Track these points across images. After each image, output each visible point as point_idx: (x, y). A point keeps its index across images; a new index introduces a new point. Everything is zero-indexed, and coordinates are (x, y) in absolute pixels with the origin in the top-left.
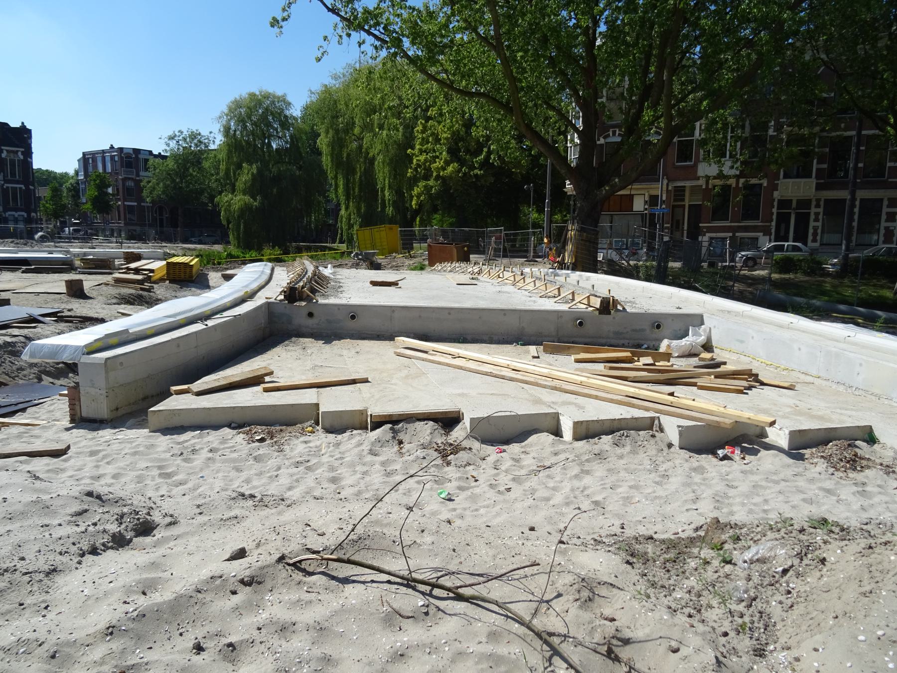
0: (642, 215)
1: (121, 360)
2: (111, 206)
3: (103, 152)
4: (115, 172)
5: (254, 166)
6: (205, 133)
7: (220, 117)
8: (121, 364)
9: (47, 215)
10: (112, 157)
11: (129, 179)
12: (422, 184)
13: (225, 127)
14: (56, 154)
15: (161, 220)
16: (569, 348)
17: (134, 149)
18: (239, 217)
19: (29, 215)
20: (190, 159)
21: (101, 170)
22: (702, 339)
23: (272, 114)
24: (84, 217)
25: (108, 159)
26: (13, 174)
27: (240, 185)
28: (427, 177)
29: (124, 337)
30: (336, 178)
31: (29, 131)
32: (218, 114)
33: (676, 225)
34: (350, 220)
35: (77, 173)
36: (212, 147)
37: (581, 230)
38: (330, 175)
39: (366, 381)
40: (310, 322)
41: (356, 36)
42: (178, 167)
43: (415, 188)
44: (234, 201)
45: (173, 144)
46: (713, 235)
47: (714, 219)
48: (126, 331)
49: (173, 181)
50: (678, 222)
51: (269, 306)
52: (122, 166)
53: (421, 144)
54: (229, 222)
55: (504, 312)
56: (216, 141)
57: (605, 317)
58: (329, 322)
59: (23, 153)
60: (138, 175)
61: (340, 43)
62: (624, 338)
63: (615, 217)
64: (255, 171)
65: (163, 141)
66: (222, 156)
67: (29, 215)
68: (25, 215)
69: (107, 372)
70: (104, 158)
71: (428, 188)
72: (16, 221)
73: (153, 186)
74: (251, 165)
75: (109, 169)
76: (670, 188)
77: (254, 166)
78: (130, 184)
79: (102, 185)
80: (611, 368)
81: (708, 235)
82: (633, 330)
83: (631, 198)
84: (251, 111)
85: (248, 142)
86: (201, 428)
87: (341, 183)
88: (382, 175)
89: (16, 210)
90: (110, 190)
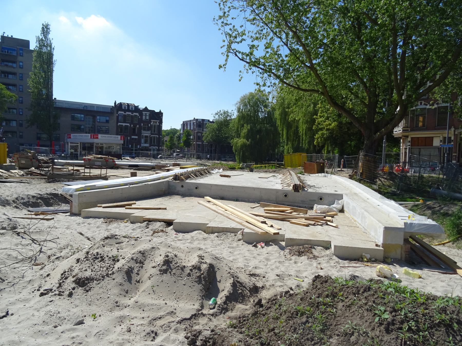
0: (439, 149)
1: (85, 194)
2: (191, 144)
3: (190, 121)
4: (194, 130)
5: (249, 126)
6: (230, 111)
7: (237, 104)
8: (85, 196)
9: (167, 148)
10: (194, 123)
11: (199, 132)
12: (320, 133)
13: (238, 108)
14: (171, 123)
15: (211, 150)
16: (269, 205)
18: (240, 148)
19: (159, 148)
20: (223, 124)
21: (189, 128)
22: (339, 207)
23: (260, 101)
24: (181, 148)
25: (192, 124)
26: (154, 131)
27: (242, 134)
28: (321, 129)
29: (93, 188)
30: (283, 130)
31: (162, 113)
32: (236, 102)
34: (288, 150)
35: (180, 130)
36: (233, 117)
37: (365, 156)
38: (280, 129)
39: (166, 209)
40: (182, 189)
41: (254, 69)
42: (218, 127)
43: (317, 135)
44: (238, 142)
45: (217, 117)
48: (95, 185)
49: (216, 133)
51: (168, 181)
52: (197, 127)
53: (321, 113)
55: (254, 189)
56: (235, 115)
57: (297, 193)
58: (189, 189)
59: (159, 122)
60: (203, 131)
61: (247, 73)
62: (306, 204)
63: (422, 149)
64: (249, 128)
65: (213, 115)
66: (237, 121)
67: (159, 148)
68: (157, 148)
69: (79, 198)
70: (190, 123)
71: (323, 134)
72: (154, 150)
73: (207, 135)
74: (247, 125)
75: (192, 128)
76: (456, 133)
77: (249, 126)
78: (199, 134)
79: (188, 135)
80: (266, 213)
82: (310, 200)
83: (431, 139)
84: (249, 100)
85: (248, 115)
86: (95, 218)
87: (285, 133)
88: (302, 127)
89: (154, 146)
90: (192, 137)
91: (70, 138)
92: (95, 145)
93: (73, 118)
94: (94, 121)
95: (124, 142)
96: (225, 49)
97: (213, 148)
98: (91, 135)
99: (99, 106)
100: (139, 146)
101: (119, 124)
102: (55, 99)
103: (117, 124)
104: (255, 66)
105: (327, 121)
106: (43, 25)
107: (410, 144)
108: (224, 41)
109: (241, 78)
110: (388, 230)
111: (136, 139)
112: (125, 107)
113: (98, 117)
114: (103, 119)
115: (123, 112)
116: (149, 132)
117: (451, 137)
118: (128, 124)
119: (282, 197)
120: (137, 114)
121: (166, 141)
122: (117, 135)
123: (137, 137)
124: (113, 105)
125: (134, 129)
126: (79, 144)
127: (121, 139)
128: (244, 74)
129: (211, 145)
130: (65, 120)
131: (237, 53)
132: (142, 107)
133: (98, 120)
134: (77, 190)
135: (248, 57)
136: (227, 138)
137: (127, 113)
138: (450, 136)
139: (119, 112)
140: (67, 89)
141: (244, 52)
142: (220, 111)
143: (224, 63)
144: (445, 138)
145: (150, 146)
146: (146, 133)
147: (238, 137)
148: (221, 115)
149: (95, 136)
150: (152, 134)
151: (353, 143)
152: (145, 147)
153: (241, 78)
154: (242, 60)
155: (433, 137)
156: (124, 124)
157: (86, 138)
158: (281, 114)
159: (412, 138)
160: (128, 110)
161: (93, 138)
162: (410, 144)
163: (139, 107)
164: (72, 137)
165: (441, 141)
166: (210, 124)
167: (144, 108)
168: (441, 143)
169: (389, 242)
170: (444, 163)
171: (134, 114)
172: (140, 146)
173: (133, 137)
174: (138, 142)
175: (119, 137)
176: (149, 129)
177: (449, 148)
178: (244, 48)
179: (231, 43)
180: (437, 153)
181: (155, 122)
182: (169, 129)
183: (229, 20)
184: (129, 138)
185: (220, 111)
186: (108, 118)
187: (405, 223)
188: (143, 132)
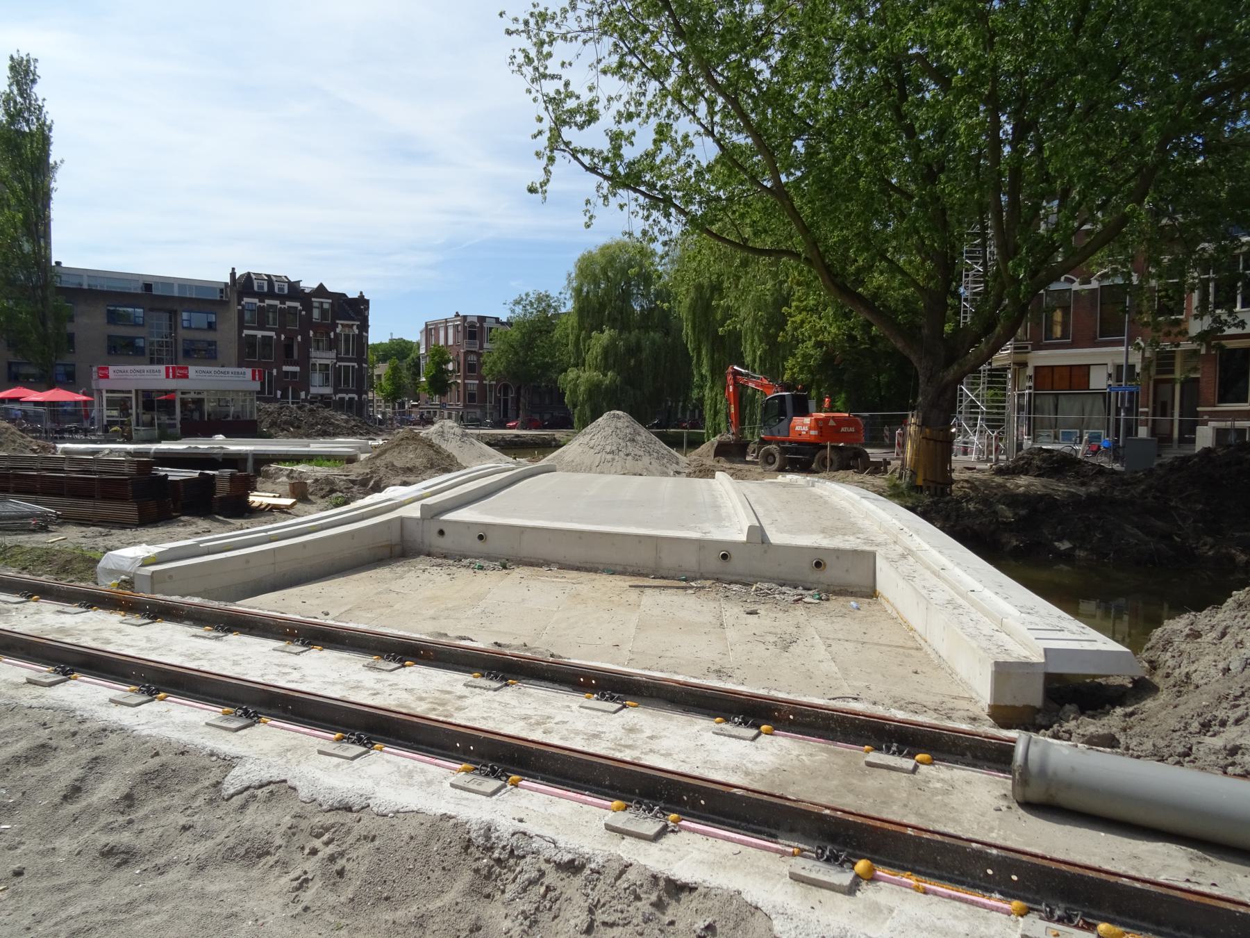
0: (1105, 396)
3: (446, 321)
6: (554, 294)
8: (171, 577)
11: (472, 352)
17: (479, 317)
20: (537, 328)
21: (442, 342)
27: (589, 358)
31: (367, 302)
33: (1162, 408)
36: (563, 310)
37: (923, 424)
41: (625, 195)
45: (519, 309)
46: (1222, 425)
47: (1223, 399)
49: (516, 353)
50: (1164, 405)
51: (402, 520)
54: (575, 406)
59: (358, 327)
60: (481, 347)
75: (451, 342)
78: (473, 358)
81: (1212, 424)
89: (347, 392)
90: (450, 366)
91: (106, 377)
92: (178, 396)
93: (113, 318)
94: (173, 326)
95: (263, 384)
96: (543, 140)
97: (511, 395)
98: (167, 369)
99: (184, 284)
100: (303, 395)
101: (246, 332)
102: (58, 263)
103: (240, 332)
104: (627, 187)
105: (817, 324)
106: (12, 58)
107: (1031, 384)
108: (540, 120)
109: (591, 217)
110: (1004, 672)
111: (296, 373)
112: (261, 287)
113: (185, 315)
114: (200, 319)
115: (256, 301)
116: (333, 354)
117: (1133, 366)
118: (273, 334)
119: (714, 564)
120: (297, 304)
121: (379, 376)
122: (240, 366)
123: (297, 369)
124: (228, 280)
125: (288, 348)
126: (133, 395)
127: (254, 378)
128: (599, 210)
129: (506, 387)
130: (90, 325)
131: (579, 156)
132: (309, 284)
133: (186, 324)
134: (146, 562)
135: (608, 165)
136: (546, 367)
137: (268, 302)
138: (1131, 361)
139: (246, 300)
140: (91, 232)
141: (597, 149)
142: (527, 295)
143: (542, 177)
144: (1119, 368)
145: (335, 393)
146: (322, 358)
147: (576, 365)
148: (531, 304)
149: (178, 372)
150: (339, 359)
151: (884, 379)
152: (322, 395)
153: (591, 217)
154: (593, 169)
155: (1088, 366)
156: (259, 334)
157: (154, 377)
158: (693, 308)
159: (1036, 368)
160: (271, 294)
161: (174, 377)
162: (1031, 384)
163: (302, 284)
164: (111, 374)
165: (1110, 375)
166: (501, 329)
167: (315, 286)
168: (1110, 382)
169: (1008, 701)
170: (1117, 435)
171: (289, 304)
172: (307, 393)
173: (285, 368)
174: (303, 382)
175: (249, 371)
176: (332, 345)
177: (1131, 393)
178: (594, 138)
179: (560, 122)
180: (1099, 402)
181: (347, 326)
182: (386, 340)
183: (553, 66)
184: (275, 372)
185: (527, 295)
186: (213, 318)
187: (1046, 650)
188: (313, 353)
